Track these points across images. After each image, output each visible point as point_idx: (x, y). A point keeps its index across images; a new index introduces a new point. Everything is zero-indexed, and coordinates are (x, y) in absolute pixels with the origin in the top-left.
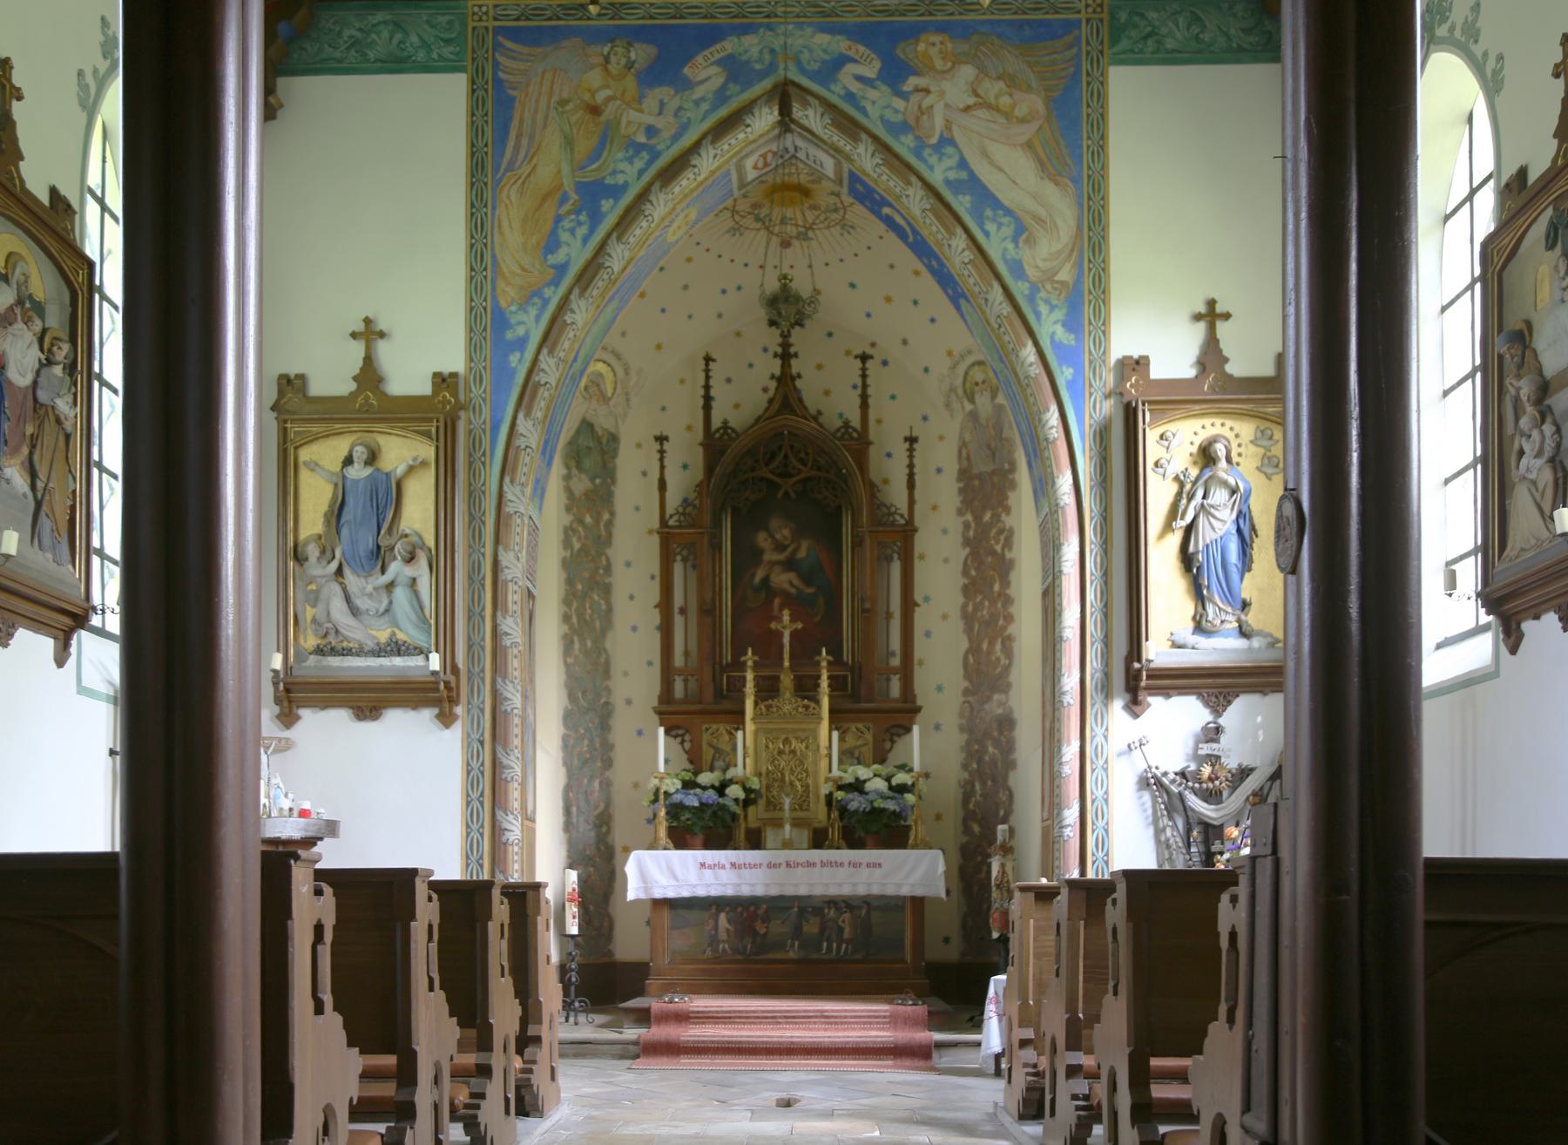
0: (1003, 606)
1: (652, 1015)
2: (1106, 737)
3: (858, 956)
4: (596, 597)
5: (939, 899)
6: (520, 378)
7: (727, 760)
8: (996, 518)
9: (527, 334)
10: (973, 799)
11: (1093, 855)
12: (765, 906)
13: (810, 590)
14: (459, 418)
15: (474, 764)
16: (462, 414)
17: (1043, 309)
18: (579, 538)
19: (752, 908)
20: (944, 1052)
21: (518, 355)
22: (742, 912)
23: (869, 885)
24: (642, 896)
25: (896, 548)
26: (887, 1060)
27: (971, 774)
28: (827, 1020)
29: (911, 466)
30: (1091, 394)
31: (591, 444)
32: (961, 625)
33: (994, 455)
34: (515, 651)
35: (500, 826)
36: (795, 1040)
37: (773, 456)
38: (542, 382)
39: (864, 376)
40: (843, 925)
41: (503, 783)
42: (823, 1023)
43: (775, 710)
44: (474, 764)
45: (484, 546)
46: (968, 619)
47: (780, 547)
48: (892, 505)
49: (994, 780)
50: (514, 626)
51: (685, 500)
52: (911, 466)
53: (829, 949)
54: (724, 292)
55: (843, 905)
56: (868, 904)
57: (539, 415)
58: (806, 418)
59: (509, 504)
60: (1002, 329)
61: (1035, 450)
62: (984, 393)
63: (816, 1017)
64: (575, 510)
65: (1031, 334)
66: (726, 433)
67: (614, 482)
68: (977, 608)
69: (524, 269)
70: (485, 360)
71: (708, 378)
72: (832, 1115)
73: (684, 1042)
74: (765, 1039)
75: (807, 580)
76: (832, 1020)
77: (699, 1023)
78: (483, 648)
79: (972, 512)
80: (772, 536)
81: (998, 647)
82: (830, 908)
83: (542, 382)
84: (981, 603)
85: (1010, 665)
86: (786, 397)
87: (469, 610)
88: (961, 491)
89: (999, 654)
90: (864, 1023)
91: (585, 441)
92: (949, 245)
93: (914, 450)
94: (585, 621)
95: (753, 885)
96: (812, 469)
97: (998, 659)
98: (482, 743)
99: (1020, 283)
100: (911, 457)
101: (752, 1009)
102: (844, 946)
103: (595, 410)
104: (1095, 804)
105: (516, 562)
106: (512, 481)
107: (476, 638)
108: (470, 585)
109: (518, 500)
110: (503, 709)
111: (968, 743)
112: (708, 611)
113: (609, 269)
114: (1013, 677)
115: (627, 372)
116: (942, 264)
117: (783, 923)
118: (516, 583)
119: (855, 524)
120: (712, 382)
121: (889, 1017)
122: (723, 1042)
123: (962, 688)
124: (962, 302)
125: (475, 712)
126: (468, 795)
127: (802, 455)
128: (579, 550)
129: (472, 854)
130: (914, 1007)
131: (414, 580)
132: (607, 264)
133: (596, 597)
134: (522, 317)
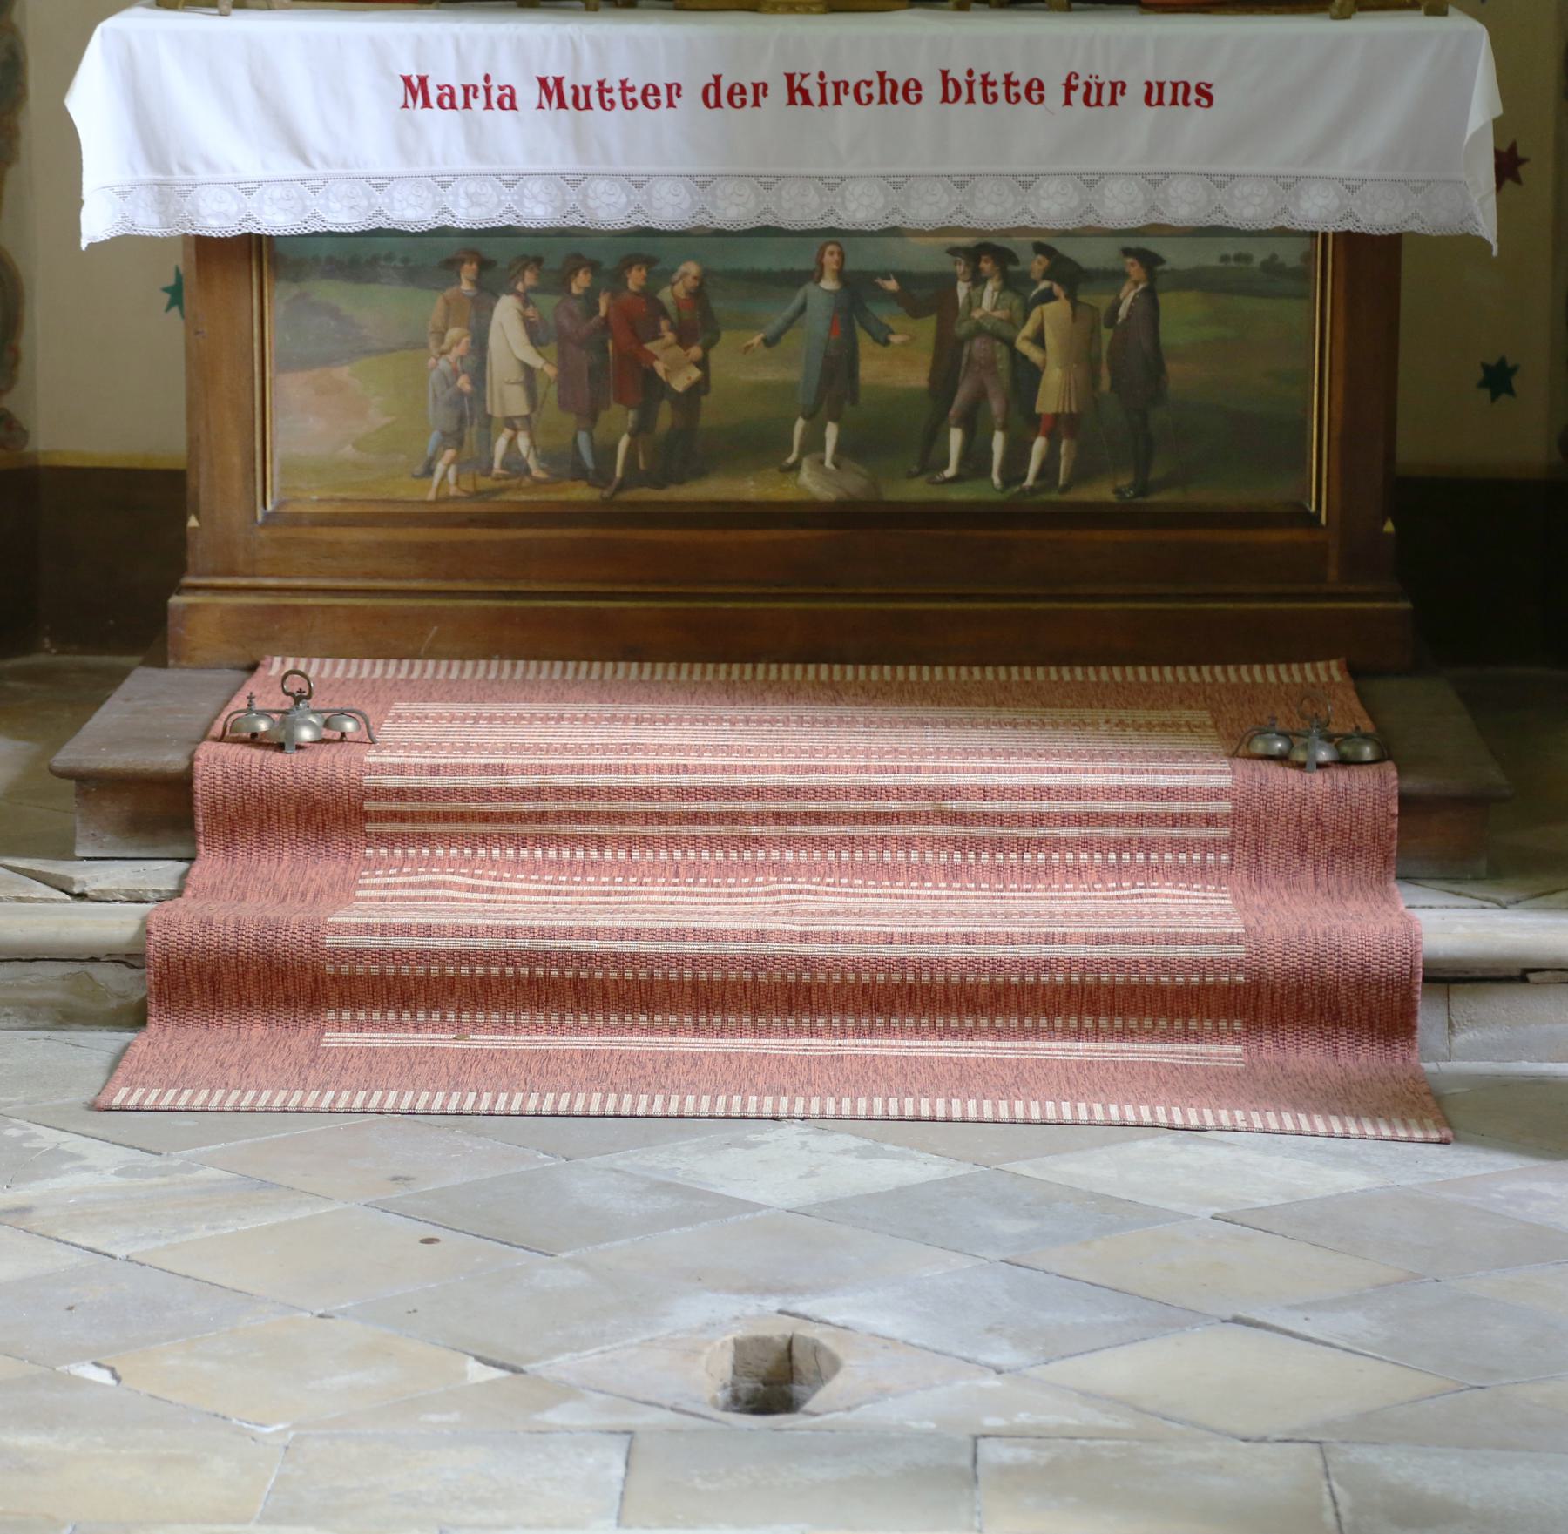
1: (200, 807)
3: (1101, 492)
5: (1471, 244)
12: (692, 268)
19: (635, 278)
20: (1466, 1003)
22: (590, 297)
23: (1155, 181)
24: (148, 224)
26: (1218, 1037)
28: (959, 831)
36: (819, 949)
40: (1034, 354)
42: (939, 843)
53: (975, 461)
55: (1038, 264)
56: (1149, 261)
63: (913, 817)
72: (972, 1479)
73: (337, 955)
74: (690, 947)
76: (981, 831)
77: (405, 839)
82: (978, 280)
90: (1121, 846)
95: (639, 183)
101: (639, 780)
102: (1039, 445)
117: (769, 342)
121: (1234, 819)
122: (508, 957)
130: (1342, 777)
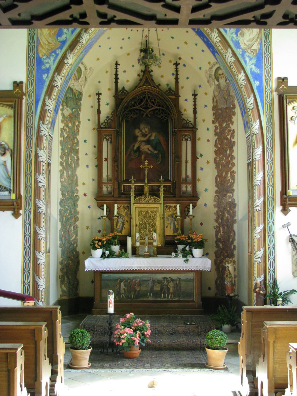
2: (273, 223)
4: (73, 155)
8: (228, 125)
9: (50, 67)
10: (220, 234)
11: (269, 269)
13: (156, 152)
14: (23, 99)
15: (27, 233)
16: (24, 97)
17: (247, 59)
18: (67, 132)
21: (46, 75)
25: (189, 136)
27: (218, 224)
29: (195, 105)
30: (266, 92)
31: (72, 96)
33: (226, 101)
34: (43, 189)
35: (37, 258)
37: (142, 101)
39: (177, 71)
40: (169, 287)
41: (38, 240)
43: (142, 200)
44: (27, 233)
45: (32, 148)
47: (144, 135)
49: (228, 227)
50: (43, 205)
51: (108, 117)
52: (195, 105)
54: (123, 39)
57: (54, 97)
58: (155, 87)
59: (42, 132)
60: (232, 67)
62: (223, 78)
64: (65, 122)
65: (243, 68)
66: (123, 92)
67: (80, 110)
68: (221, 159)
69: (49, 42)
70: (33, 77)
71: (117, 71)
75: (155, 148)
78: (31, 187)
79: (219, 123)
80: (141, 131)
81: (229, 175)
82: (164, 280)
83: (55, 85)
84: (222, 157)
86: (147, 79)
87: (26, 173)
88: (214, 114)
89: (229, 178)
92: (211, 35)
93: (196, 99)
94: (69, 164)
96: (156, 106)
97: (229, 180)
98: (30, 225)
99: (238, 50)
102: (170, 295)
103: (73, 83)
104: (270, 249)
105: (44, 154)
106: (43, 123)
107: (28, 184)
108: (26, 163)
109: (45, 130)
110: (38, 211)
111: (217, 212)
112: (116, 160)
114: (235, 187)
115: (86, 69)
118: (44, 162)
120: (118, 73)
123: (215, 190)
124: (216, 54)
125: (28, 212)
126: (24, 245)
127: (153, 100)
129: (26, 268)
131: (5, 161)
132: (81, 41)
133: (73, 155)
134: (48, 60)
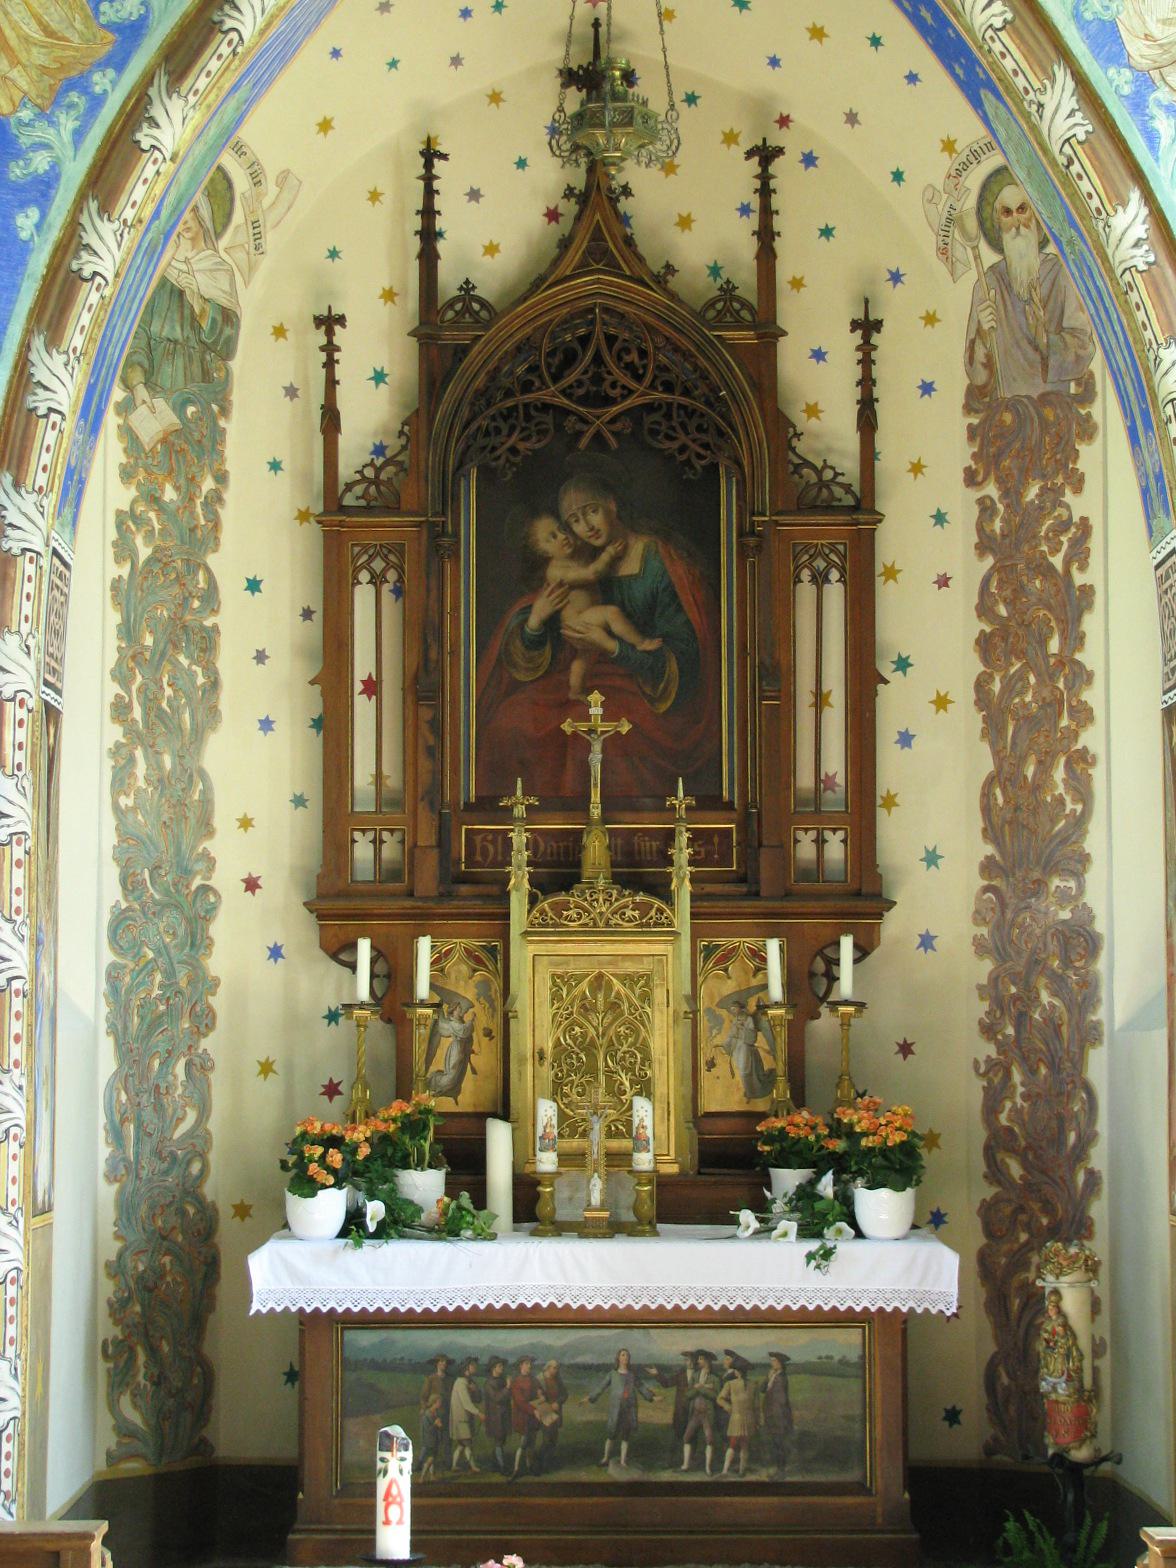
0: (1069, 688)
4: (183, 660)
6: (38, 263)
7: (468, 1018)
8: (1052, 496)
10: (1008, 1104)
18: (150, 534)
21: (34, 213)
27: (1001, 1048)
29: (867, 382)
31: (178, 334)
32: (977, 720)
34: (18, 852)
37: (570, 359)
38: (86, 273)
39: (765, 192)
40: (726, 1407)
46: (993, 712)
47: (584, 552)
48: (826, 466)
49: (1054, 1066)
52: (867, 382)
55: (727, 1361)
59: (9, 532)
60: (1075, 168)
61: (1145, 415)
64: (141, 476)
65: (1138, 176)
66: (467, 309)
71: (430, 193)
80: (566, 527)
81: (1059, 774)
82: (697, 1368)
84: (1021, 676)
85: (1086, 815)
86: (597, 236)
88: (972, 433)
89: (1061, 789)
91: (168, 328)
96: (652, 387)
97: (1060, 801)
99: (1112, 72)
100: (867, 362)
102: (729, 1452)
103: (187, 261)
105: (22, 657)
111: (995, 979)
113: (234, 36)
115: (256, 179)
116: (944, 22)
118: (22, 703)
119: (747, 508)
120: (439, 203)
124: (987, 97)
127: (634, 357)
128: (148, 561)
132: (229, 24)
133: (183, 660)
134: (42, 132)
